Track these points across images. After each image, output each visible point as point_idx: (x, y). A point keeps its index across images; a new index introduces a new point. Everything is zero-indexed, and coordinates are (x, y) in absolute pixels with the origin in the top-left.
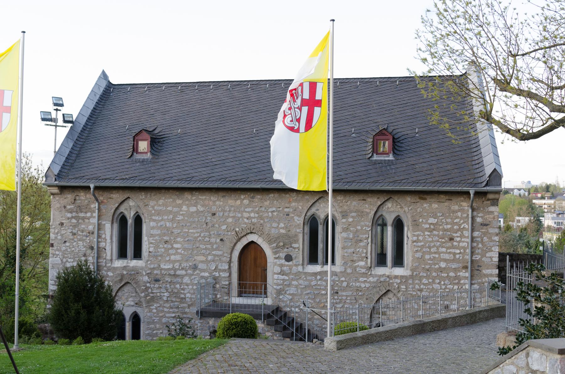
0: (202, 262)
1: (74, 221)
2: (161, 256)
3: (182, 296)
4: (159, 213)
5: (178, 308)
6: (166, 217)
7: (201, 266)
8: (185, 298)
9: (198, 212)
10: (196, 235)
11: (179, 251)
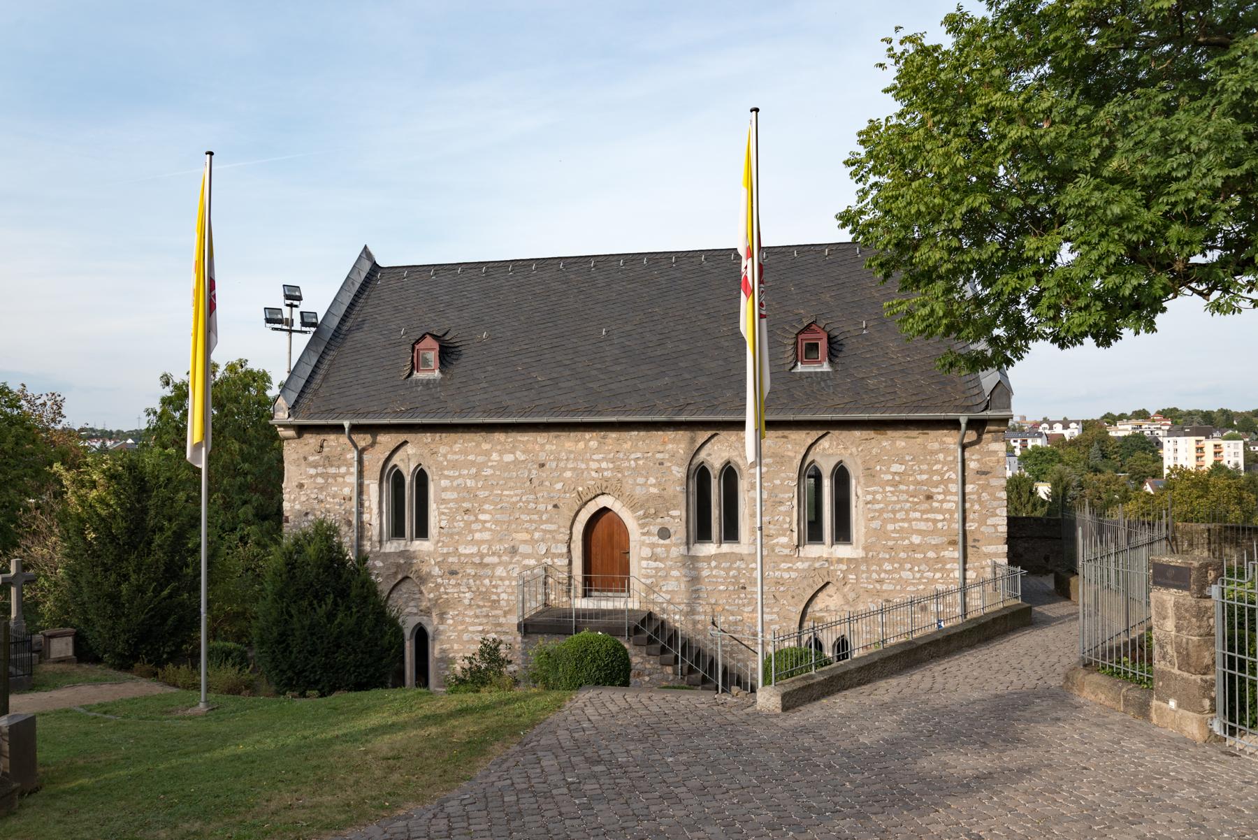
0: (525, 542)
1: (320, 480)
2: (459, 533)
3: (494, 597)
4: (454, 465)
5: (487, 616)
6: (466, 472)
7: (523, 549)
8: (498, 601)
9: (516, 462)
10: (514, 499)
11: (488, 525)
